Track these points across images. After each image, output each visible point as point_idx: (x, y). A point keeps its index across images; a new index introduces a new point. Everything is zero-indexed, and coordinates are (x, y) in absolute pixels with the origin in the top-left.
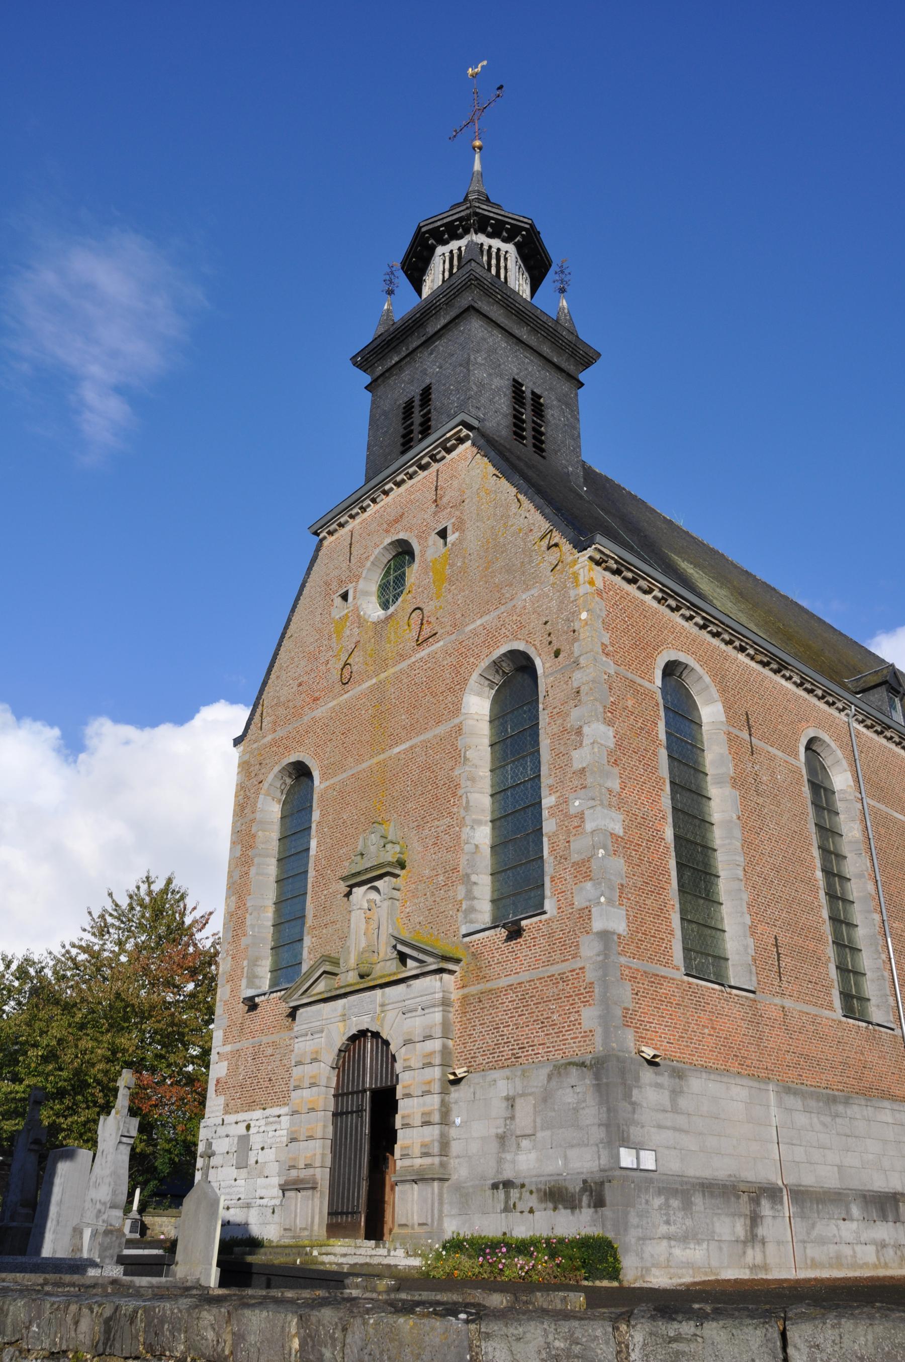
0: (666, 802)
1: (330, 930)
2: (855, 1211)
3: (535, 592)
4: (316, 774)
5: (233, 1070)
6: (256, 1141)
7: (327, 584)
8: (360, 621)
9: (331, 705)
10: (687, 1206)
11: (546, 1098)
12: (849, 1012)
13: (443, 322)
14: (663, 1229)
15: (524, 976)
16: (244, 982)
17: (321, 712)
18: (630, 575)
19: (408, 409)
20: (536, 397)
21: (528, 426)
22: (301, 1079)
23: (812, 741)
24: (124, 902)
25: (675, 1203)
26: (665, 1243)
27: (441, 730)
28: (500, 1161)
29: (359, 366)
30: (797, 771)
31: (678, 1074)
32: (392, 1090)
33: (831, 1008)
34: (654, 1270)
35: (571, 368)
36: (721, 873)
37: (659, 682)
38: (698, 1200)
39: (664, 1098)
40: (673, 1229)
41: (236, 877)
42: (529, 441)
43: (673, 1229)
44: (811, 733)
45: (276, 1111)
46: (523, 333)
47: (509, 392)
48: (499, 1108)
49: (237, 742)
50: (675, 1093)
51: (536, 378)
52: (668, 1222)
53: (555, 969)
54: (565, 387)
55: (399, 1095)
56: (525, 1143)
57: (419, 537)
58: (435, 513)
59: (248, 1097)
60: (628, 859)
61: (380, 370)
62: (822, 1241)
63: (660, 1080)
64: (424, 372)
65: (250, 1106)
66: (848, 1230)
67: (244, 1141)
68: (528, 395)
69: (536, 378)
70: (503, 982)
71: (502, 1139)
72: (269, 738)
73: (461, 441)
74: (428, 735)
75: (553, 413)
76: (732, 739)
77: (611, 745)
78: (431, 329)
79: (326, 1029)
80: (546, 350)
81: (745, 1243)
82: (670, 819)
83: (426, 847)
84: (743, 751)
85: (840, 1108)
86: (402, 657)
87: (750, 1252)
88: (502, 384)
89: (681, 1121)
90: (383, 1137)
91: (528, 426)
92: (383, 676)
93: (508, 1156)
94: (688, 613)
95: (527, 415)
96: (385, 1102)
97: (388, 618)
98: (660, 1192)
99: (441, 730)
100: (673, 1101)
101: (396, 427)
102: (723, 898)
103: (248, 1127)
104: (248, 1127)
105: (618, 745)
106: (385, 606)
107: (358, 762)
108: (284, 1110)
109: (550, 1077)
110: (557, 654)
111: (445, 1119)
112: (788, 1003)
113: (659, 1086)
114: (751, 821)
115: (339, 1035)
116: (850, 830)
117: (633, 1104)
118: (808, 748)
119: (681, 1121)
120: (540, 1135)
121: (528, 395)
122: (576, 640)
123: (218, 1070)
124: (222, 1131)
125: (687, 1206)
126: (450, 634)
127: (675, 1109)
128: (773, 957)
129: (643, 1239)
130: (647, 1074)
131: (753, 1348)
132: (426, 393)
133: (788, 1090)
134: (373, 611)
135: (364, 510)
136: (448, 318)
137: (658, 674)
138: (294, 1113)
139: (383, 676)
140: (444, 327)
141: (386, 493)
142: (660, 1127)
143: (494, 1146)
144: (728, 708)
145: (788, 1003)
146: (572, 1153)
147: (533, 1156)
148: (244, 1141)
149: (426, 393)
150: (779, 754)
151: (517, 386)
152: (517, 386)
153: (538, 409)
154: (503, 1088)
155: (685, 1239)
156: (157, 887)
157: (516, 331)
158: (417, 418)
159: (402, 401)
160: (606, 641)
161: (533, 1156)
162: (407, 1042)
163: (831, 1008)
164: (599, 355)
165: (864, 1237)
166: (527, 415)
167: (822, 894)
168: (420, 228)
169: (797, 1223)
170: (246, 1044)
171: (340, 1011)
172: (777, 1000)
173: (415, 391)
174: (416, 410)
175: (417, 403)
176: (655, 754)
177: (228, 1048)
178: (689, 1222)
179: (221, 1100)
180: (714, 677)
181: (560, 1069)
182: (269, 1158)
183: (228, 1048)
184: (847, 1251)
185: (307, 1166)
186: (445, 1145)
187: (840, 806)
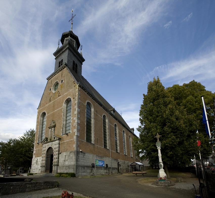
0: (86, 120)
1: (47, 134)
2: (103, 169)
3: (72, 90)
4: (46, 114)
5: (36, 152)
6: (38, 161)
7: (48, 87)
8: (52, 93)
9: (48, 104)
10: (84, 168)
11: (69, 155)
12: (105, 147)
13: (65, 49)
14: (81, 171)
15: (68, 141)
16: (37, 141)
17: (47, 105)
18: (84, 89)
19: (60, 62)
20: (76, 64)
21: (75, 68)
22: (55, 154)
23: (115, 124)
24: (28, 132)
25: (83, 168)
26: (81, 173)
27: (60, 108)
28: (64, 163)
29: (54, 55)
30: (102, 119)
31: (84, 153)
32: (53, 154)
33: (103, 147)
34: (80, 176)
35: (81, 61)
36: (92, 130)
37: (86, 104)
38: (85, 168)
39: (82, 156)
40: (82, 171)
41: (37, 127)
42: (75, 70)
43: (82, 171)
44: (104, 114)
45: (40, 157)
46: (75, 54)
47: (73, 62)
48: (64, 157)
49: (37, 109)
50: (84, 155)
51: (77, 62)
52: (82, 170)
53: (71, 140)
54: (80, 64)
55: (54, 155)
56: (67, 161)
57: (59, 81)
58: (61, 78)
59: (38, 156)
60: (80, 126)
61: (57, 56)
62: (99, 172)
63: (82, 154)
64: (62, 57)
65: (38, 157)
66: (102, 171)
67: (37, 161)
68: (75, 63)
69: (77, 62)
70: (66, 141)
71: (64, 160)
72: (41, 108)
73: (65, 67)
74: (59, 109)
75: (78, 67)
76: (94, 113)
77: (79, 111)
78: (63, 51)
79: (46, 147)
80: (78, 57)
81: (91, 172)
82: (86, 122)
83: (58, 124)
84: (96, 115)
85: (103, 158)
86: (57, 98)
87: (91, 173)
88: (72, 61)
89: (84, 159)
90: (52, 160)
91: (75, 68)
92: (54, 100)
93: (65, 163)
94: (91, 96)
95: (75, 66)
96: (52, 156)
97: (55, 92)
98: (81, 167)
99: (60, 108)
100: (84, 156)
101: (58, 65)
102: (92, 133)
103: (37, 159)
104: (37, 159)
105: (80, 112)
106: (55, 91)
107: (51, 112)
108: (41, 157)
109: (70, 153)
110: (74, 98)
111: (58, 158)
112: (98, 146)
113: (82, 154)
114: (95, 123)
115: (47, 148)
116: (107, 127)
117: (79, 156)
118: (115, 125)
119: (84, 159)
120: (68, 160)
121: (75, 63)
122: (76, 97)
123: (34, 152)
124: (35, 160)
125: (84, 168)
126: (62, 95)
127: (84, 157)
128: (96, 140)
129: (78, 172)
130: (80, 153)
131: (182, 165)
132: (62, 60)
133: (97, 156)
134: (54, 92)
135: (53, 77)
136: (65, 49)
137: (86, 103)
138: (42, 157)
139: (54, 100)
140: (65, 50)
141: (56, 74)
142: (82, 159)
143: (63, 161)
144: (94, 109)
145: (98, 146)
146: (72, 162)
147: (67, 163)
148: (37, 161)
149: (62, 60)
150: (100, 116)
151: (74, 62)
152: (74, 62)
153: (76, 66)
154: (65, 154)
155: (84, 172)
156: (32, 130)
157: (74, 53)
158: (61, 63)
159: (59, 61)
160: (80, 97)
161: (67, 163)
162: (55, 149)
163: (103, 147)
164: (85, 60)
165: (104, 171)
166: (75, 66)
167: (103, 133)
168: (63, 34)
169: (97, 171)
170: (38, 149)
171: (48, 144)
172: (97, 145)
173: (61, 60)
174: (61, 62)
175: (61, 62)
176: (85, 114)
177: (36, 149)
178: (84, 170)
179: (35, 156)
180: (93, 105)
181: (71, 152)
182: (40, 163)
183: (36, 149)
184: (102, 173)
185: (43, 164)
186: (58, 161)
187: (106, 124)
